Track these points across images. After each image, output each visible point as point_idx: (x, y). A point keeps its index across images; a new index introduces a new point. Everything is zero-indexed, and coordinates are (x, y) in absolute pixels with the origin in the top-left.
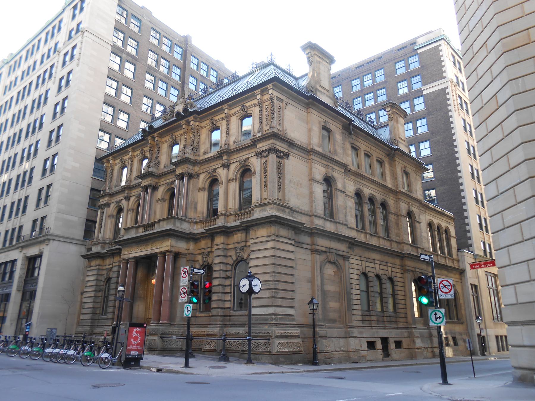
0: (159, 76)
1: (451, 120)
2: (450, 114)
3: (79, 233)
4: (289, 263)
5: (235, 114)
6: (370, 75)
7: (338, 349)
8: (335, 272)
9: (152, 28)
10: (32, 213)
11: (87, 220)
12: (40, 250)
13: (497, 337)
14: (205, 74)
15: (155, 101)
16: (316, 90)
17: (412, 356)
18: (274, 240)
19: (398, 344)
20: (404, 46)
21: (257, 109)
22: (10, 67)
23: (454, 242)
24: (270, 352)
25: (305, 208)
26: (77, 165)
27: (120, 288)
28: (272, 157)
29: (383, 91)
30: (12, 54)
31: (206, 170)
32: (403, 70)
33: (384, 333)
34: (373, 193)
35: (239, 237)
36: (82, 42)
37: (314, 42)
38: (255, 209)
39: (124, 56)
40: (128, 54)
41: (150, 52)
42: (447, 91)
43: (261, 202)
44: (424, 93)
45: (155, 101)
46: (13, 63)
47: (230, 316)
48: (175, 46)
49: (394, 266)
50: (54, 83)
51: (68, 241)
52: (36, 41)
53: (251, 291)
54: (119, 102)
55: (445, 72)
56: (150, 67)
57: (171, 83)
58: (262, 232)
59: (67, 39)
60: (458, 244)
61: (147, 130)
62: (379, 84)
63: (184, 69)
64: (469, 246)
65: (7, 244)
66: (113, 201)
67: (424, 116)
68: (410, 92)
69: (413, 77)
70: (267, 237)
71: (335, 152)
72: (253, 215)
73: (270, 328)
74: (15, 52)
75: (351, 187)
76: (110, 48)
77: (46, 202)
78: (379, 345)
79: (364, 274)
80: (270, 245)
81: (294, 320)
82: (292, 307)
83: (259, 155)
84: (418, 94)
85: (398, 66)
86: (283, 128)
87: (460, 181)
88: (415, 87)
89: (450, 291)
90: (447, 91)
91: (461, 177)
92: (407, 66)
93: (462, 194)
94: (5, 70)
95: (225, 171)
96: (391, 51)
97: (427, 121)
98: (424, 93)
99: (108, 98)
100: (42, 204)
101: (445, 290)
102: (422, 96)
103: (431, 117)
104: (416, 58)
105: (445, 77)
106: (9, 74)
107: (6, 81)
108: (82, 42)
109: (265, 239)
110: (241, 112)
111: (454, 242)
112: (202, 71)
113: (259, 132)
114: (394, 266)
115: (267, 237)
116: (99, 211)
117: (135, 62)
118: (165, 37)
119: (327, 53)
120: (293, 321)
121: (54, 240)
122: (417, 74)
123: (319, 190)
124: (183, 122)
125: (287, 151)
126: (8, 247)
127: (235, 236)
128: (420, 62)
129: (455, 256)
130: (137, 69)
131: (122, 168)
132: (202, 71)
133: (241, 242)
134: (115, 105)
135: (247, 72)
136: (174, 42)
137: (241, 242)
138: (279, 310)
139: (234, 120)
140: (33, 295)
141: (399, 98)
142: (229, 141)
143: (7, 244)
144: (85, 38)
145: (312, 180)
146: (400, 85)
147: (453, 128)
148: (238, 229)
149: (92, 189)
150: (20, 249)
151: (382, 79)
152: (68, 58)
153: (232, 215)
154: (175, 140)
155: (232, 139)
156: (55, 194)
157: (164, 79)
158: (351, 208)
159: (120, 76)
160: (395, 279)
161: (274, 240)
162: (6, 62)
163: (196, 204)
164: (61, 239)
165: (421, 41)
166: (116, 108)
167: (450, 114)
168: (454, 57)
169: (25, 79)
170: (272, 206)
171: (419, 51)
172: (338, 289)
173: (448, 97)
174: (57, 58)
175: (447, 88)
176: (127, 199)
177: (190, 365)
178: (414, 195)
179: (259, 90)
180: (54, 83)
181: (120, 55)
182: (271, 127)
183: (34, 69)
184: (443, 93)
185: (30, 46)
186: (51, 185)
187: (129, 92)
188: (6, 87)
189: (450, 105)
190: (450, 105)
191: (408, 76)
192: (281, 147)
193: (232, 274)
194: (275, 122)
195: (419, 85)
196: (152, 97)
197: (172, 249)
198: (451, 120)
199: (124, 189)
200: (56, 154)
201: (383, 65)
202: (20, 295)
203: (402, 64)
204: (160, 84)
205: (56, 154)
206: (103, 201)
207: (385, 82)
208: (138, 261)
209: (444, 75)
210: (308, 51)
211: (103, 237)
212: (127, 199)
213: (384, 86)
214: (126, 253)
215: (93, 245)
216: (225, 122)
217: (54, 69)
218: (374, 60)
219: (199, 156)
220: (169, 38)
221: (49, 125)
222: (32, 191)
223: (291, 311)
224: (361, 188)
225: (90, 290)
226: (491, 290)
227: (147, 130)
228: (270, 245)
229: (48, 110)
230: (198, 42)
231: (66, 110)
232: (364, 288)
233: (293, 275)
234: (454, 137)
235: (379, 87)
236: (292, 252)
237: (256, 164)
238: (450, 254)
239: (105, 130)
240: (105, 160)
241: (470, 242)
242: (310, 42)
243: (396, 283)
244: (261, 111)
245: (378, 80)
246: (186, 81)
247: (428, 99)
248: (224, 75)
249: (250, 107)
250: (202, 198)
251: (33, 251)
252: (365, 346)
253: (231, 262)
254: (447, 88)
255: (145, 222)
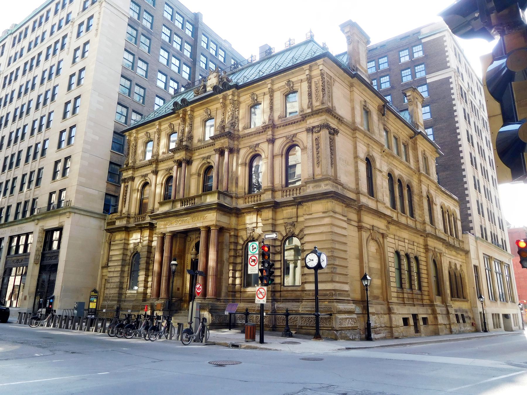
0: (173, 52)
1: (455, 108)
2: (454, 102)
3: (99, 207)
4: (343, 239)
5: (279, 89)
6: (374, 62)
7: (383, 325)
8: (377, 249)
9: (166, 4)
10: (47, 184)
11: (106, 194)
12: (59, 223)
13: (493, 314)
14: (214, 53)
15: (169, 77)
16: (357, 68)
17: (436, 333)
18: (332, 216)
19: (425, 320)
20: (407, 35)
21: (305, 85)
22: (15, 38)
23: (459, 224)
24: (334, 327)
25: (352, 186)
26: (97, 138)
27: (173, 262)
28: (324, 133)
29: (387, 79)
30: (16, 25)
31: (248, 145)
32: (407, 59)
33: (414, 310)
34: (401, 174)
35: (288, 212)
36: (100, 13)
37: (354, 21)
38: (308, 185)
39: (140, 29)
40: (144, 28)
41: (164, 27)
42: (451, 80)
43: (314, 178)
44: (428, 81)
45: (169, 78)
46: (18, 34)
47: (280, 291)
48: (187, 23)
49: (419, 245)
50: (68, 54)
51: (89, 214)
52: (44, 12)
53: (319, 266)
54: (136, 76)
55: (449, 62)
56: (164, 42)
57: (183, 60)
58: (318, 207)
59: (81, 9)
60: (462, 226)
61: (180, 103)
62: (382, 71)
63: (194, 46)
64: (470, 229)
65: (20, 216)
66: (137, 175)
67: (428, 103)
68: (414, 80)
69: (417, 66)
70: (324, 212)
71: (373, 133)
72: (304, 190)
73: (330, 304)
74: (19, 21)
75: (385, 169)
76: (127, 20)
77: (64, 174)
78: (411, 322)
79: (397, 253)
80: (327, 221)
81: (348, 296)
82: (347, 283)
83: (310, 130)
84: (423, 82)
85: (402, 54)
86: (332, 104)
87: (463, 167)
88: (418, 76)
89: (264, 297)
90: (451, 80)
91: (463, 163)
92: (411, 55)
93: (465, 180)
94: (9, 41)
95: (270, 146)
96: (395, 40)
97: (430, 108)
98: (428, 81)
99: (125, 70)
100: (59, 176)
101: (260, 296)
102: (426, 84)
103: (434, 104)
104: (420, 47)
105: (449, 67)
106: (14, 45)
107: (9, 52)
108: (100, 13)
109: (321, 215)
110: (287, 87)
111: (459, 224)
112: (211, 50)
113: (309, 108)
114: (419, 245)
115: (324, 212)
116: (123, 185)
117: (150, 36)
118: (177, 13)
119: (364, 32)
120: (348, 297)
121: (75, 213)
122: (421, 62)
123: (362, 168)
124: (220, 96)
125: (337, 128)
126: (21, 220)
127: (285, 212)
128: (424, 51)
129: (460, 238)
130: (152, 43)
131: (147, 143)
132: (211, 50)
133: (292, 218)
134: (131, 78)
135: (283, 48)
136: (186, 18)
137: (292, 218)
138: (338, 286)
139: (278, 97)
140: (54, 268)
141: (402, 86)
142: (273, 116)
143: (20, 216)
144: (103, 9)
145: (356, 157)
146: (404, 73)
147: (456, 116)
148: (288, 204)
149: (111, 163)
150: (36, 221)
151: (386, 66)
152: (84, 28)
153: (279, 191)
154: (210, 115)
155: (276, 115)
156: (74, 167)
157: (177, 55)
158: (386, 188)
159: (136, 50)
160: (420, 258)
161: (332, 216)
162: (10, 32)
163: (237, 179)
164: (82, 213)
165: (425, 31)
166: (133, 82)
167: (454, 102)
168: (455, 49)
169: (32, 50)
170: (327, 182)
171: (423, 41)
172: (379, 267)
173: (451, 86)
174: (70, 28)
175: (451, 77)
176: (156, 173)
177: (265, 341)
178: (431, 178)
179: (308, 65)
180: (68, 54)
181: (136, 27)
182: (323, 103)
183: (42, 40)
184: (446, 82)
185: (38, 17)
186: (70, 157)
187: (144, 67)
188: (10, 58)
189: (453, 94)
190: (453, 94)
191: (413, 64)
192: (333, 123)
193: (281, 249)
194: (326, 98)
195: (423, 74)
196: (166, 73)
197: (218, 224)
198: (455, 108)
199: (150, 163)
200: (74, 126)
201: (386, 53)
202: (37, 268)
203: (406, 52)
204: (174, 60)
205: (74, 126)
206: (126, 175)
207: (389, 69)
208: (175, 235)
209: (448, 64)
210: (347, 30)
211: (129, 210)
212: (156, 173)
213: (388, 73)
214: (162, 227)
215: (117, 219)
216: (267, 97)
217: (67, 40)
218: (377, 48)
219: (238, 131)
220: (181, 14)
221: (62, 96)
222: (47, 164)
223: (346, 287)
224: (393, 168)
225: (116, 264)
226: (487, 271)
227: (180, 103)
228: (327, 221)
229: (62, 81)
230: (208, 21)
231: (82, 81)
232: (397, 267)
233: (346, 251)
234: (457, 125)
235: (383, 74)
236: (345, 228)
237: (305, 139)
238: (457, 237)
239: (123, 103)
240: (127, 134)
241: (471, 225)
242: (350, 21)
243: (420, 262)
244: (310, 87)
245: (382, 67)
246: (197, 59)
247: (431, 87)
248: (231, 55)
249: (297, 82)
250: (242, 172)
251: (51, 223)
252: (401, 322)
253: (280, 238)
254: (451, 77)
255: (181, 195)
